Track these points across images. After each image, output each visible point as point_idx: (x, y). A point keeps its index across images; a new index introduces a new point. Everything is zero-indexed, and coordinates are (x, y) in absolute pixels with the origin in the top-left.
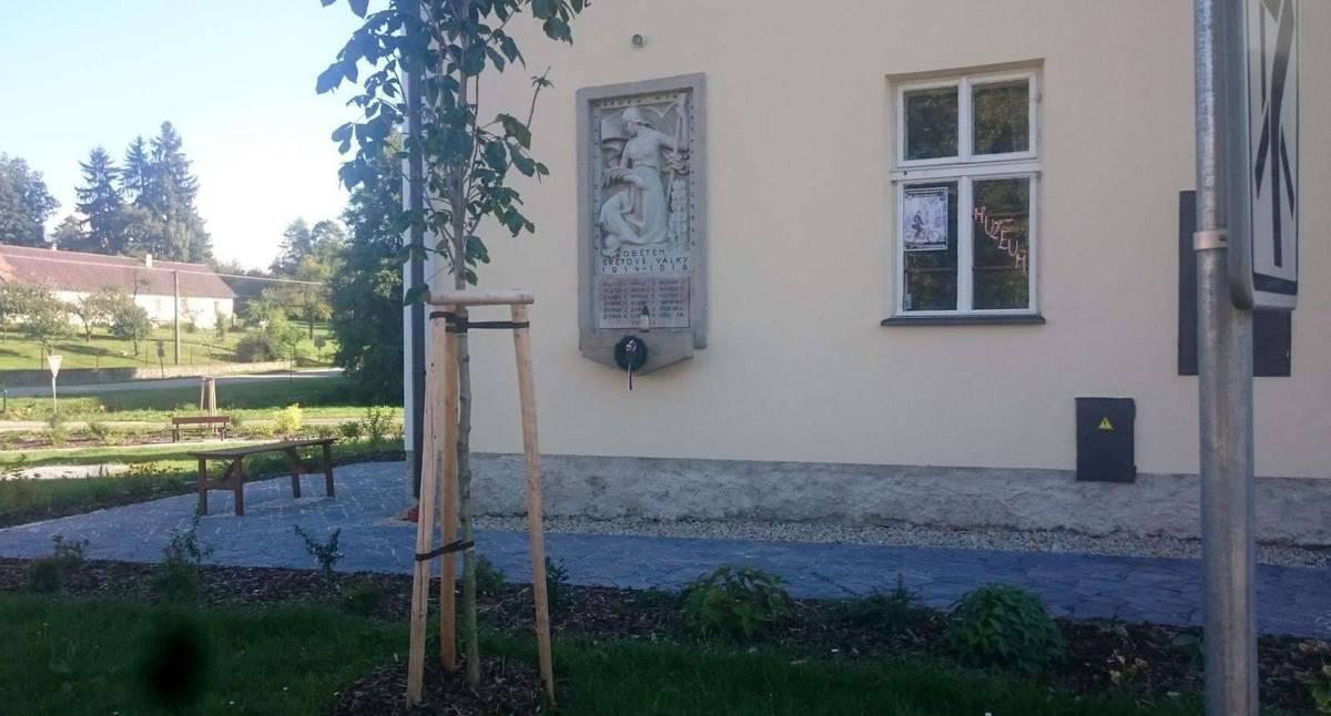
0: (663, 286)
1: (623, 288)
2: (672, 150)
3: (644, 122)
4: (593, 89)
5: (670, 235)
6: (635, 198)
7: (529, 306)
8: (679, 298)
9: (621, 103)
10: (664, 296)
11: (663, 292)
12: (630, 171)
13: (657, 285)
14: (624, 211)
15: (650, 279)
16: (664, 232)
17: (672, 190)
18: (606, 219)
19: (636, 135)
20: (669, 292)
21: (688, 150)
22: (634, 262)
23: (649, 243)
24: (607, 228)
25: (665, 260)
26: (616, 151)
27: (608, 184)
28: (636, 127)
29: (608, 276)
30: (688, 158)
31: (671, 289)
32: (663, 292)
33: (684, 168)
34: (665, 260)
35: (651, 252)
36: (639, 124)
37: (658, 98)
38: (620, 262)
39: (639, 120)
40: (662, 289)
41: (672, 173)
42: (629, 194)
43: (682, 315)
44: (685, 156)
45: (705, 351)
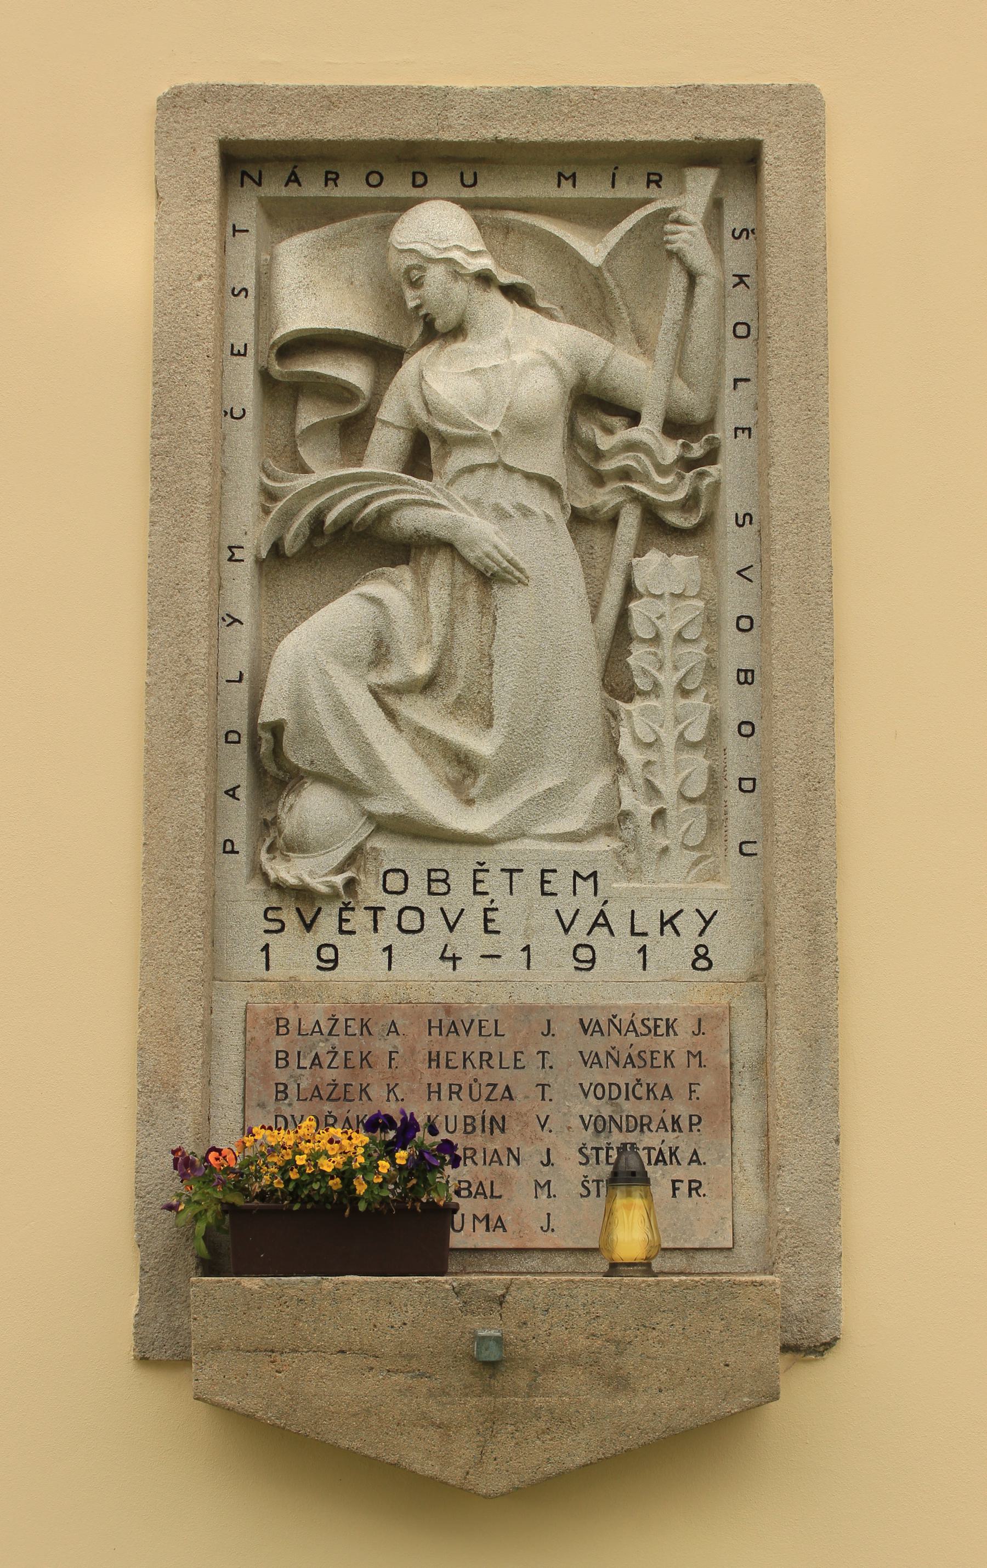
0: (598, 1044)
1: (381, 1046)
2: (634, 418)
3: (505, 278)
4: (253, 94)
5: (628, 802)
6: (451, 622)
7: (609, 183)
8: (681, 1108)
9: (331, 178)
10: (600, 1091)
11: (596, 1075)
12: (416, 488)
13: (567, 1028)
14: (393, 675)
15: (528, 1010)
16: (598, 782)
17: (630, 592)
18: (300, 703)
19: (458, 331)
20: (626, 1076)
21: (709, 424)
22: (434, 921)
23: (518, 834)
24: (296, 756)
25: (602, 921)
26: (343, 392)
27: (291, 545)
28: (460, 290)
29: (290, 985)
30: (711, 457)
31: (645, 1060)
32: (596, 1075)
33: (691, 503)
34: (602, 921)
35: (528, 881)
36: (484, 279)
37: (294, 179)
38: (360, 919)
39: (485, 262)
40: (590, 1060)
41: (630, 521)
42: (419, 602)
43: (694, 1188)
44: (697, 450)
45: (831, 1359)
